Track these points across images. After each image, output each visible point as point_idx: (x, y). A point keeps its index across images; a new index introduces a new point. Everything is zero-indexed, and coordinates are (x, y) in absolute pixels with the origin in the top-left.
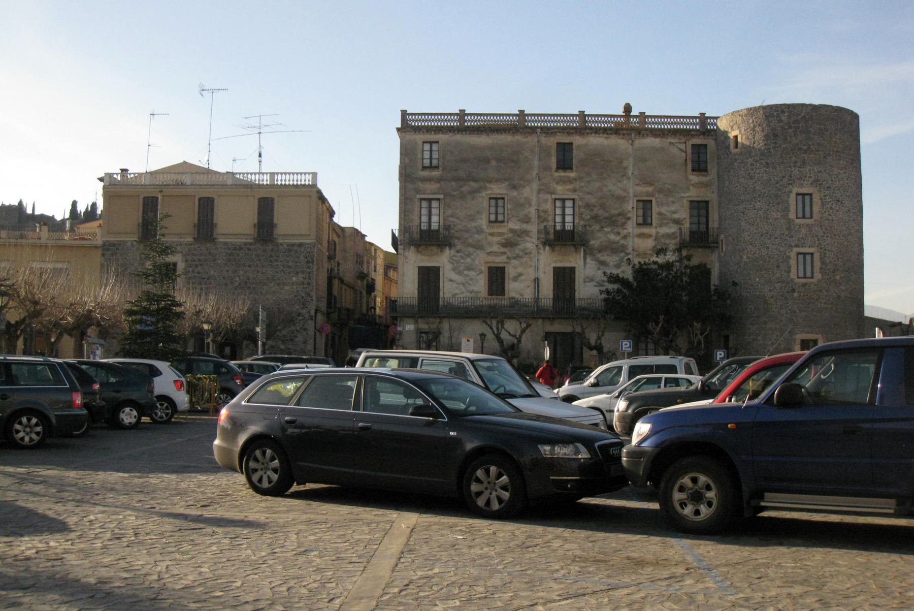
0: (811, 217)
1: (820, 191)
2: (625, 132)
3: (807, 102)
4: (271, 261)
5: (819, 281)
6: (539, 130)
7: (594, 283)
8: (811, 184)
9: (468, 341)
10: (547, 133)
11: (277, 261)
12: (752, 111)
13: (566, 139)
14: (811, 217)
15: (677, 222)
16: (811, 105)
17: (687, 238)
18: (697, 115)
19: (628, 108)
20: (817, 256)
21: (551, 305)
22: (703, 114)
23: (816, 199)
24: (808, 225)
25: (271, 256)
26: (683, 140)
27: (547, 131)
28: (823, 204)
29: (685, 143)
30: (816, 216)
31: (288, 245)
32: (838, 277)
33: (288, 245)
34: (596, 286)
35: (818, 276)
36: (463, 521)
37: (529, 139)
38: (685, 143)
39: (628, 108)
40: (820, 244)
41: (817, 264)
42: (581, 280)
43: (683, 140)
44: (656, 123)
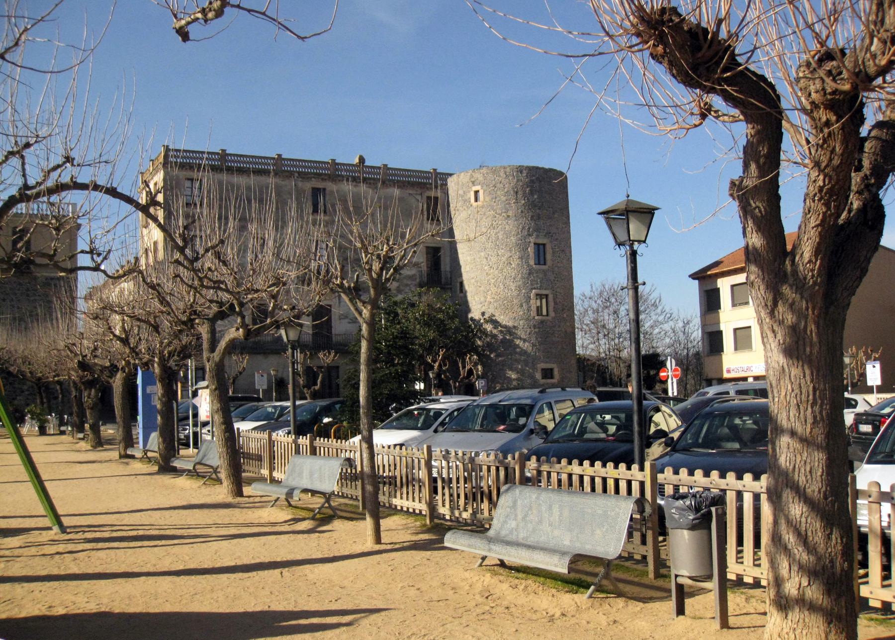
0: (545, 264)
1: (551, 242)
2: (372, 182)
3: (540, 166)
4: (28, 295)
5: (553, 318)
6: (296, 175)
7: (347, 320)
8: (545, 236)
9: (262, 376)
10: (303, 178)
11: (35, 295)
12: (520, 169)
13: (320, 185)
14: (545, 264)
15: (416, 265)
16: (543, 168)
17: (425, 280)
18: (218, 150)
19: (362, 160)
20: (551, 297)
21: (311, 340)
22: (224, 151)
23: (548, 247)
24: (543, 271)
25: (28, 290)
26: (419, 192)
27: (304, 176)
28: (554, 253)
29: (421, 194)
30: (549, 262)
31: (46, 279)
32: (565, 316)
33: (46, 279)
34: (349, 323)
35: (552, 314)
36: (504, 551)
37: (286, 182)
38: (421, 194)
39: (362, 160)
40: (553, 287)
41: (551, 304)
42: (337, 317)
43: (419, 192)
44: (236, 162)
